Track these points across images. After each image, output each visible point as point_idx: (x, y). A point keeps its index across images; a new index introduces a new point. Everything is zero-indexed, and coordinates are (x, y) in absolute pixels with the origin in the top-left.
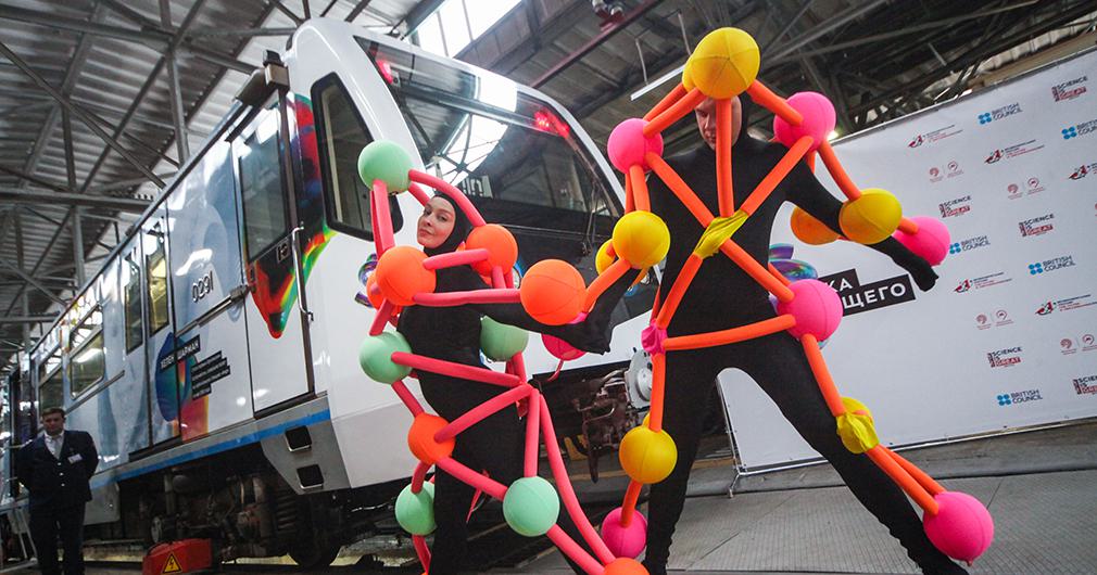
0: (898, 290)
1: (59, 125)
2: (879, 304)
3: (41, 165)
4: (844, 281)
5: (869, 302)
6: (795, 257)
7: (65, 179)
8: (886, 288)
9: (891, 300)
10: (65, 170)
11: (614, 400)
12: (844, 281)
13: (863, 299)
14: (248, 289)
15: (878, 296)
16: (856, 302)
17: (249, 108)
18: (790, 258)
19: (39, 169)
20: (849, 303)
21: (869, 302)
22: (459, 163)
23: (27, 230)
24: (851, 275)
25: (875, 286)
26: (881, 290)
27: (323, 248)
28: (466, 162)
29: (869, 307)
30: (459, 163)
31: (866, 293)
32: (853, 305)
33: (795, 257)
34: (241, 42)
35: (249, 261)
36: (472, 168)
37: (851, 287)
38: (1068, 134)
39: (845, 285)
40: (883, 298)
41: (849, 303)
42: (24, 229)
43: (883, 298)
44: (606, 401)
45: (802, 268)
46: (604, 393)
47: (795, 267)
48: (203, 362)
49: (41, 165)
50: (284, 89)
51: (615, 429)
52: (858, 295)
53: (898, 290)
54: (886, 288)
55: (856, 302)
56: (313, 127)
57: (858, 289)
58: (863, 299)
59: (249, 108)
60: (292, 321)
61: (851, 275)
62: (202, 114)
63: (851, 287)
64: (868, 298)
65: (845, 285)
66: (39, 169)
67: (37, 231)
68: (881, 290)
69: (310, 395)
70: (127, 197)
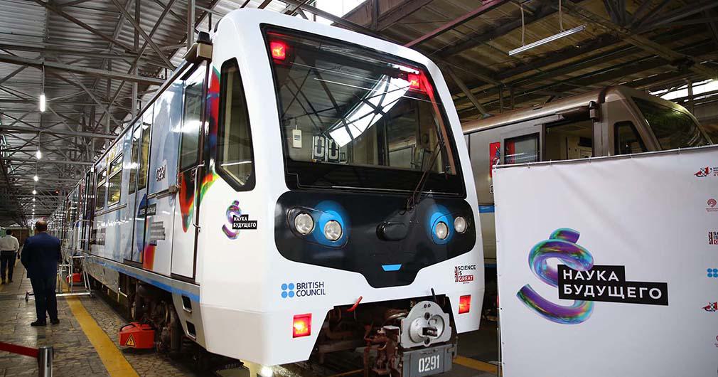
0: (655, 293)
1: (133, 8)
2: (637, 300)
3: (124, 26)
4: (613, 273)
5: (629, 296)
6: (579, 243)
7: (133, 44)
8: (646, 289)
9: (646, 300)
10: (133, 40)
11: (388, 339)
12: (613, 273)
13: (625, 292)
14: (178, 189)
15: (637, 293)
16: (619, 293)
17: (192, 65)
18: (575, 243)
19: (119, 38)
20: (613, 293)
21: (629, 296)
22: (376, 106)
23: (115, 65)
24: (620, 270)
25: (637, 285)
26: (641, 289)
27: (210, 185)
28: (383, 105)
29: (628, 300)
30: (376, 106)
31: (629, 288)
32: (616, 295)
33: (579, 243)
34: (203, 14)
35: (181, 170)
36: (386, 110)
37: (617, 280)
38: (432, 290)
39: (613, 276)
40: (641, 296)
41: (613, 293)
42: (113, 65)
43: (641, 296)
44: (383, 338)
45: (583, 253)
46: (382, 332)
47: (577, 251)
48: (157, 223)
49: (124, 26)
50: (209, 61)
51: (387, 358)
52: (621, 288)
53: (655, 293)
54: (646, 289)
55: (619, 293)
56: (219, 95)
57: (623, 283)
58: (625, 292)
59: (192, 65)
60: (192, 221)
61: (620, 270)
62: (174, 58)
63: (617, 280)
64: (629, 292)
65: (613, 276)
66: (119, 38)
67: (68, 29)
68: (641, 289)
69: (192, 280)
70: (155, 77)
